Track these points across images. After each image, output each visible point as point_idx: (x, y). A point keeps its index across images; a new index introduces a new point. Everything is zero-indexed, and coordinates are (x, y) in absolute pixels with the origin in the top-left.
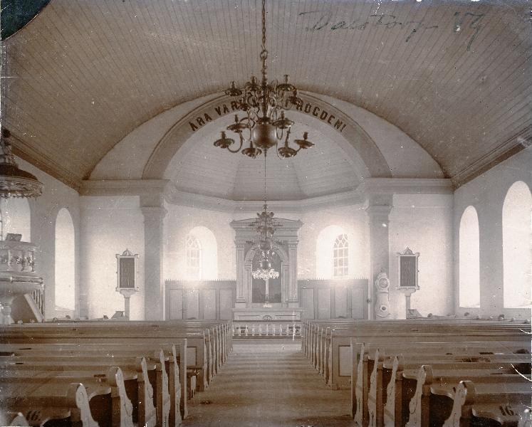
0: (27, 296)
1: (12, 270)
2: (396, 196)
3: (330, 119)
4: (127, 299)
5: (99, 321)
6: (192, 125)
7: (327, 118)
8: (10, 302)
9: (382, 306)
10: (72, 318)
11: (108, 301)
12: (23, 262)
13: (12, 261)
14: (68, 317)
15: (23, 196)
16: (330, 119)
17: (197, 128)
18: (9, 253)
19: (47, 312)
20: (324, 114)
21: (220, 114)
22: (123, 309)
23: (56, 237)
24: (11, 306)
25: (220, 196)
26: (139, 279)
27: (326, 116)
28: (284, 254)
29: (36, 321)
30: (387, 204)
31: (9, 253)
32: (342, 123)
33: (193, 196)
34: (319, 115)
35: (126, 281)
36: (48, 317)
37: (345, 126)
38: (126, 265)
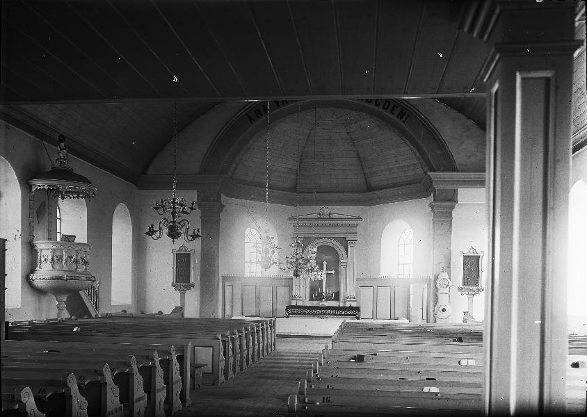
0: (82, 293)
1: (67, 269)
2: (460, 191)
3: (393, 109)
4: (183, 298)
5: (153, 316)
6: (250, 118)
7: (390, 108)
8: (65, 299)
9: (442, 308)
10: (129, 311)
11: (164, 299)
12: (76, 262)
13: (66, 260)
14: (124, 311)
15: (78, 197)
16: (393, 109)
17: (262, 115)
18: (64, 253)
19: (101, 305)
20: (387, 104)
21: (278, 106)
22: (179, 305)
23: (113, 231)
24: (65, 302)
25: (550, 392)
26: (195, 276)
27: (384, 105)
28: (344, 252)
29: (90, 316)
30: (452, 199)
31: (64, 253)
32: (405, 113)
33: (251, 190)
34: (381, 106)
35: (182, 278)
36: (103, 310)
37: (408, 116)
38: (183, 261)
